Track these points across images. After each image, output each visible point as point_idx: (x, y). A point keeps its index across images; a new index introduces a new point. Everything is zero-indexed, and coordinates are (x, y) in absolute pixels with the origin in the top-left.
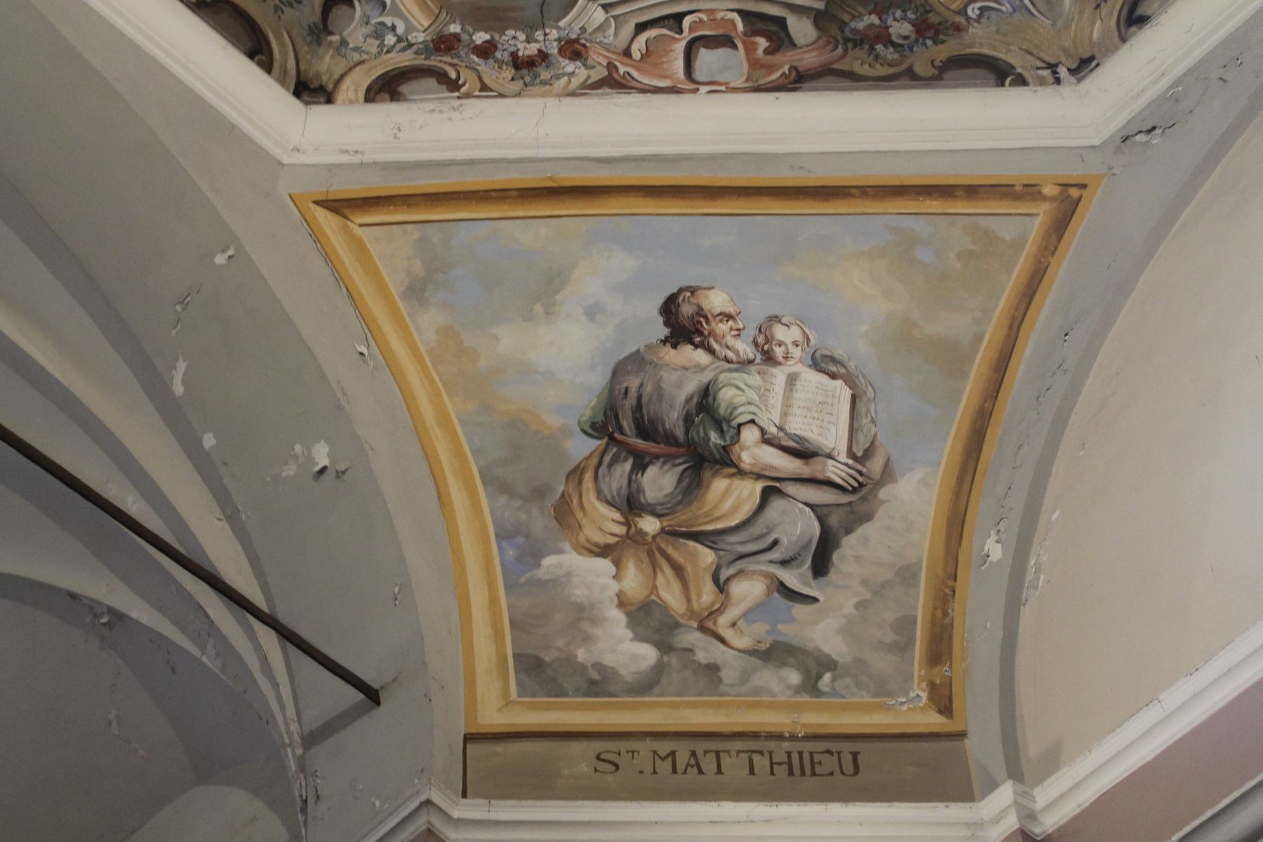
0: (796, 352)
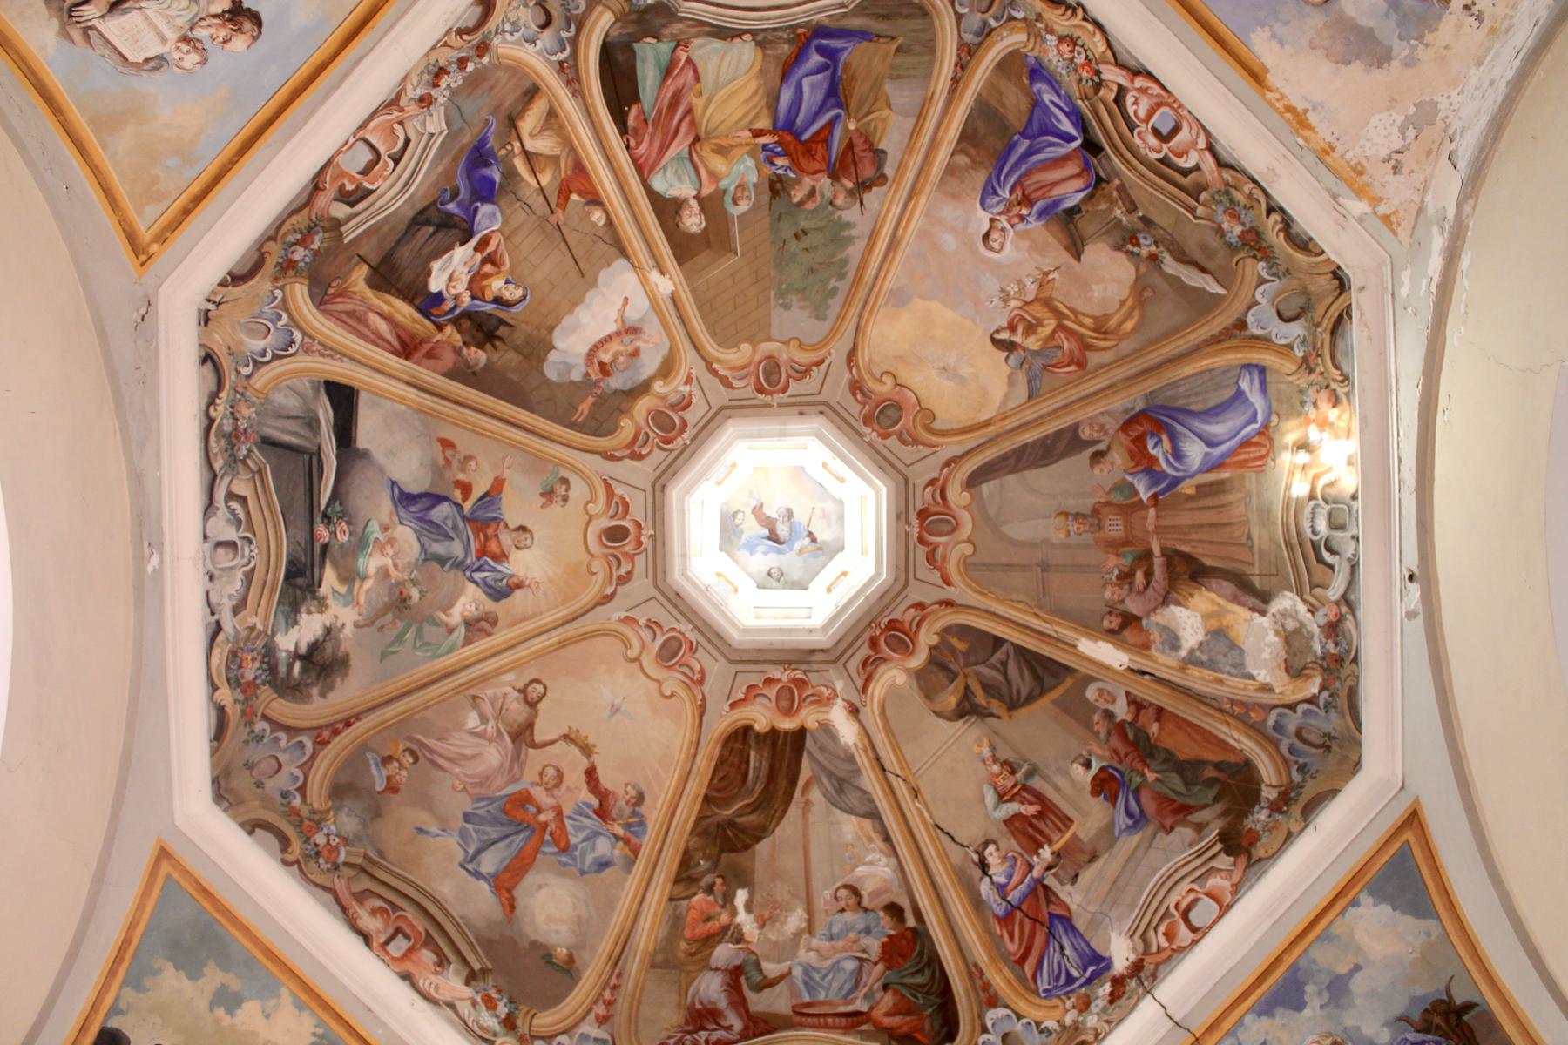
0: (177, 55)
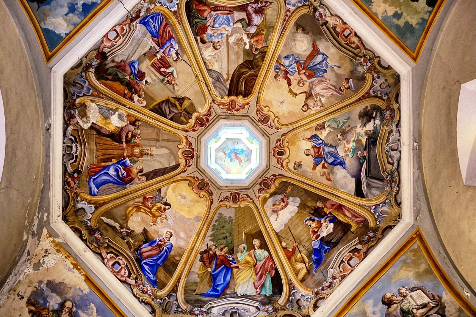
0: (407, 292)
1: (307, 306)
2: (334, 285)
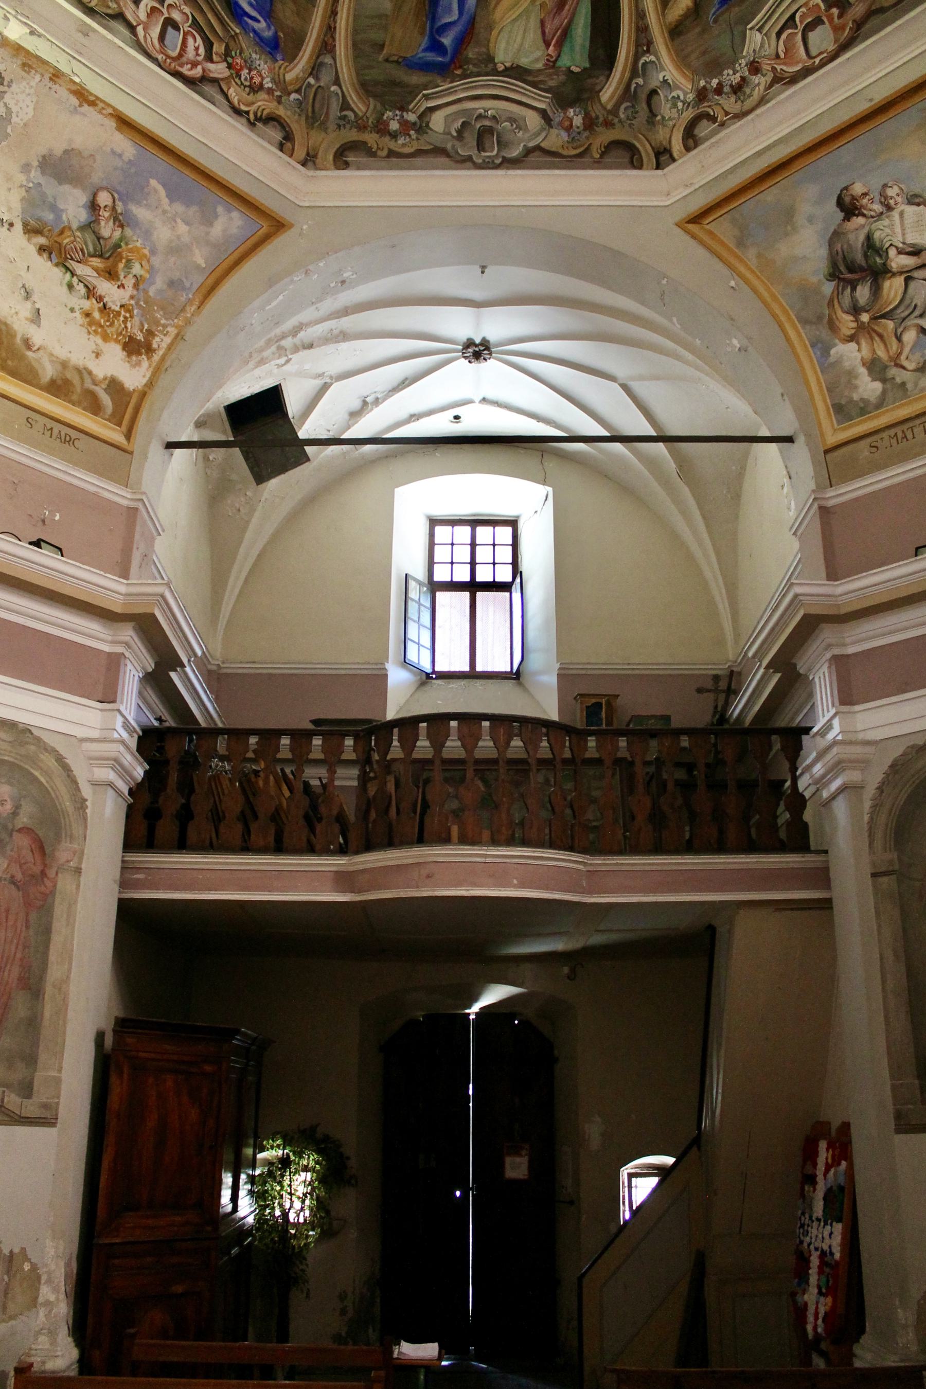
0: (899, 199)
1: (671, 123)
2: (748, 91)
